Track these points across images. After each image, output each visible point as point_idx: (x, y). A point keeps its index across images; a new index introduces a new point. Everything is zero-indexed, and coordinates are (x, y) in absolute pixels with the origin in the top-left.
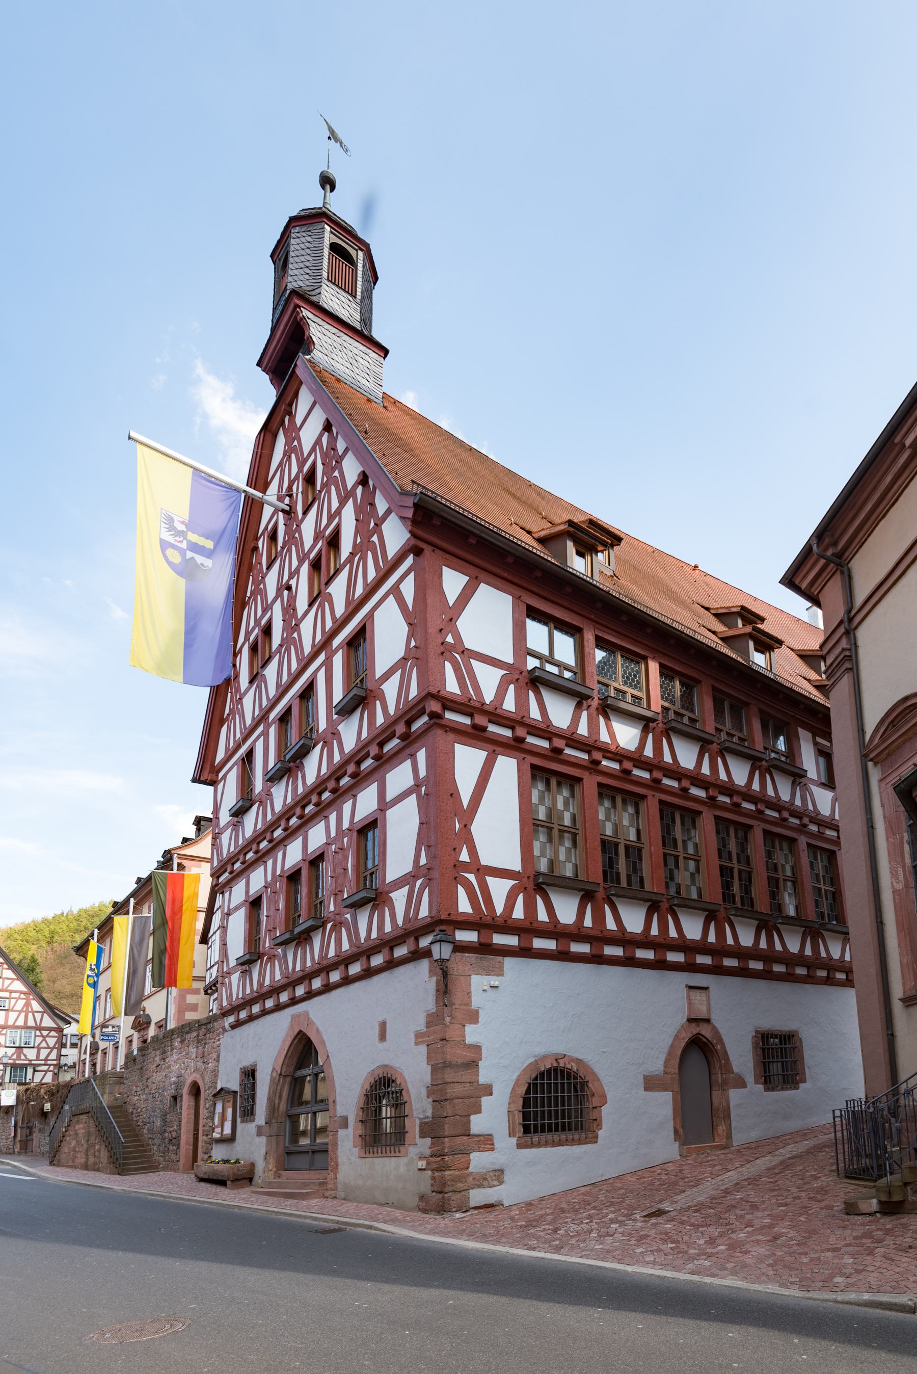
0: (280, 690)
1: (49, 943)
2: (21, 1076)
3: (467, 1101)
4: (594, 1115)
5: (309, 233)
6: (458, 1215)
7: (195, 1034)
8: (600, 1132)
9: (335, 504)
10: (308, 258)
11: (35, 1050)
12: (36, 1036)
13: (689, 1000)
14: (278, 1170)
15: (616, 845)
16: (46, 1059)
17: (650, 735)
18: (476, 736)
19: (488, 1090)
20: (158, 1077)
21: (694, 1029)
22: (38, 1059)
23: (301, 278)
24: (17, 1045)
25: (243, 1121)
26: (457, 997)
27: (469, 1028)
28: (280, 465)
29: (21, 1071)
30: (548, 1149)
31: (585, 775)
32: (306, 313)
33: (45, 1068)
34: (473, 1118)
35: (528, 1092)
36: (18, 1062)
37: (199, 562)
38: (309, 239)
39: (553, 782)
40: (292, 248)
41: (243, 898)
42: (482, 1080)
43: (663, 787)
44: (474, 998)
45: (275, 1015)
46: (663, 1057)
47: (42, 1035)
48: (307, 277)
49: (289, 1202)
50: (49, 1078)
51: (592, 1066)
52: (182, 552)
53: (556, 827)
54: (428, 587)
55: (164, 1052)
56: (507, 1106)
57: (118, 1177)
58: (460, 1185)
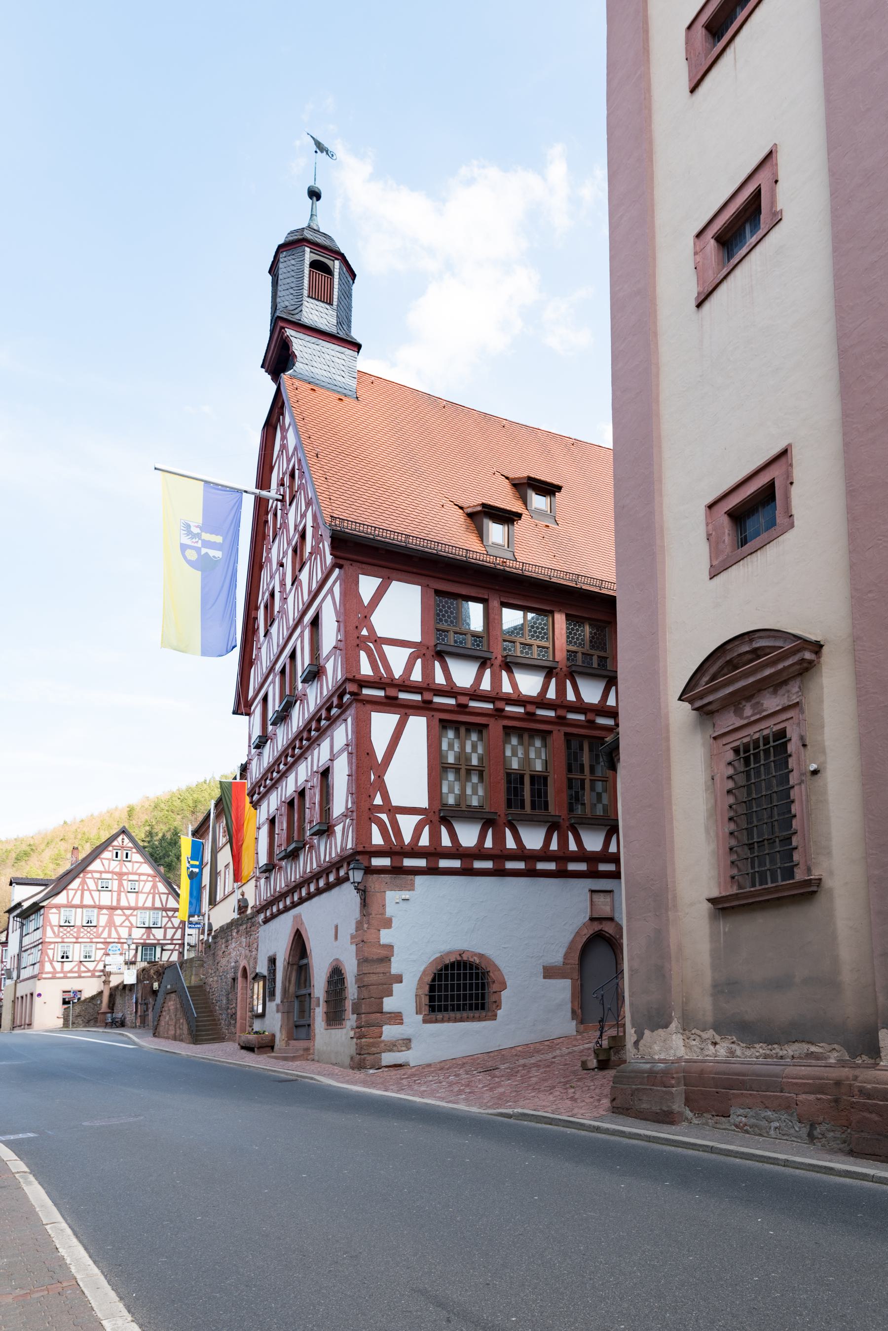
0: (279, 649)
1: (193, 813)
2: (151, 954)
3: (380, 987)
4: (493, 998)
5: (293, 257)
6: (371, 1071)
7: (244, 926)
8: (499, 1012)
9: (304, 508)
10: (293, 279)
11: (162, 930)
12: (162, 917)
13: (592, 901)
14: (289, 1039)
15: (522, 777)
16: (172, 939)
17: (554, 680)
18: (390, 704)
19: (399, 979)
20: (223, 962)
21: (597, 927)
22: (165, 939)
23: (287, 298)
24: (147, 925)
25: (270, 1000)
26: (374, 909)
27: (383, 932)
28: (278, 456)
29: (151, 950)
30: (451, 1024)
31: (491, 722)
32: (289, 332)
33: (171, 947)
34: (385, 1000)
35: (434, 980)
36: (148, 941)
37: (211, 555)
38: (293, 262)
39: (462, 730)
40: (280, 272)
41: (266, 817)
42: (394, 970)
43: (568, 722)
44: (388, 909)
45: (285, 915)
46: (562, 951)
47: (168, 916)
48: (291, 297)
49: (282, 1063)
50: (175, 957)
51: (494, 960)
52: (198, 550)
53: (463, 767)
54: (350, 591)
55: (227, 941)
56: (415, 990)
57: (192, 1045)
58: (373, 1049)
